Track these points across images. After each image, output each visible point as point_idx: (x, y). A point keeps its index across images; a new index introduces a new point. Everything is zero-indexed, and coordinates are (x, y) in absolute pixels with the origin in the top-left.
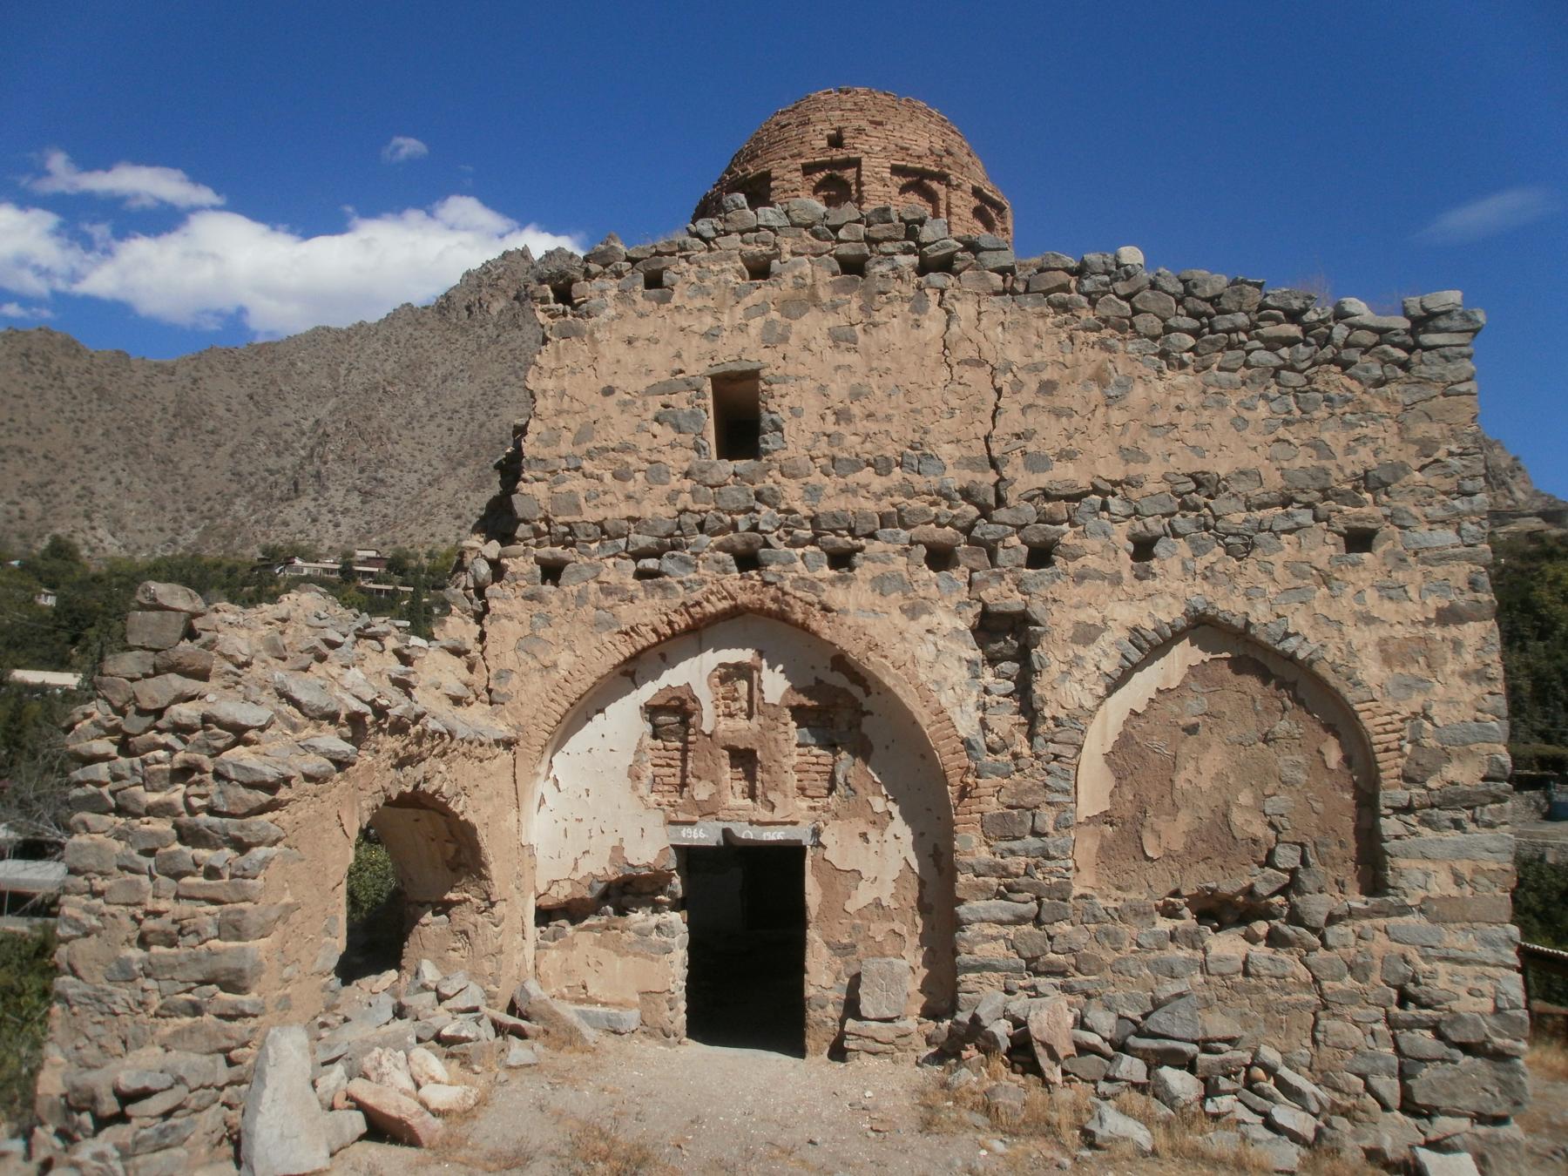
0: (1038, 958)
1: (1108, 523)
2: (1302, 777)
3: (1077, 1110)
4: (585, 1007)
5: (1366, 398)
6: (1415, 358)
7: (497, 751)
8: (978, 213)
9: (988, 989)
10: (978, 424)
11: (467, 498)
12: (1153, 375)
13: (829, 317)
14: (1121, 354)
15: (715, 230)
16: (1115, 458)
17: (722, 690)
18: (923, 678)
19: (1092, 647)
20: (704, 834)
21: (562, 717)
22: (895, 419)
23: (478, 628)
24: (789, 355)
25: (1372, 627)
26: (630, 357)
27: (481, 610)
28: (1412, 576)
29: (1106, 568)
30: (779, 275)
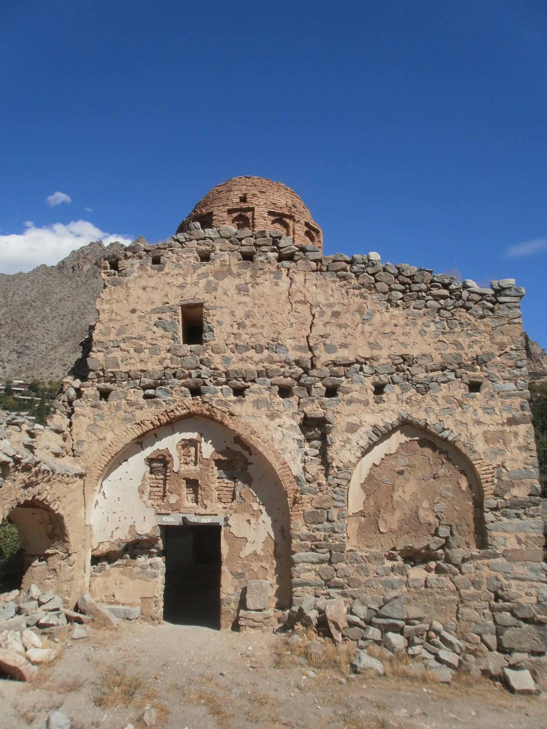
0: (330, 580)
1: (363, 377)
2: (450, 494)
3: (349, 655)
4: (113, 606)
5: (476, 323)
6: (496, 307)
7: (76, 479)
8: (307, 234)
9: (307, 595)
10: (304, 330)
11: (69, 356)
12: (384, 310)
13: (236, 280)
14: (369, 300)
15: (185, 238)
16: (367, 348)
17: (183, 452)
18: (276, 447)
19: (355, 434)
20: (174, 520)
21: (108, 463)
22: (265, 327)
23: (69, 420)
24: (217, 296)
25: (481, 426)
26: (144, 296)
27: (71, 412)
28: (497, 403)
29: (362, 398)
30: (214, 260)
